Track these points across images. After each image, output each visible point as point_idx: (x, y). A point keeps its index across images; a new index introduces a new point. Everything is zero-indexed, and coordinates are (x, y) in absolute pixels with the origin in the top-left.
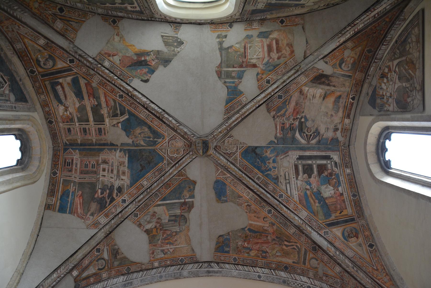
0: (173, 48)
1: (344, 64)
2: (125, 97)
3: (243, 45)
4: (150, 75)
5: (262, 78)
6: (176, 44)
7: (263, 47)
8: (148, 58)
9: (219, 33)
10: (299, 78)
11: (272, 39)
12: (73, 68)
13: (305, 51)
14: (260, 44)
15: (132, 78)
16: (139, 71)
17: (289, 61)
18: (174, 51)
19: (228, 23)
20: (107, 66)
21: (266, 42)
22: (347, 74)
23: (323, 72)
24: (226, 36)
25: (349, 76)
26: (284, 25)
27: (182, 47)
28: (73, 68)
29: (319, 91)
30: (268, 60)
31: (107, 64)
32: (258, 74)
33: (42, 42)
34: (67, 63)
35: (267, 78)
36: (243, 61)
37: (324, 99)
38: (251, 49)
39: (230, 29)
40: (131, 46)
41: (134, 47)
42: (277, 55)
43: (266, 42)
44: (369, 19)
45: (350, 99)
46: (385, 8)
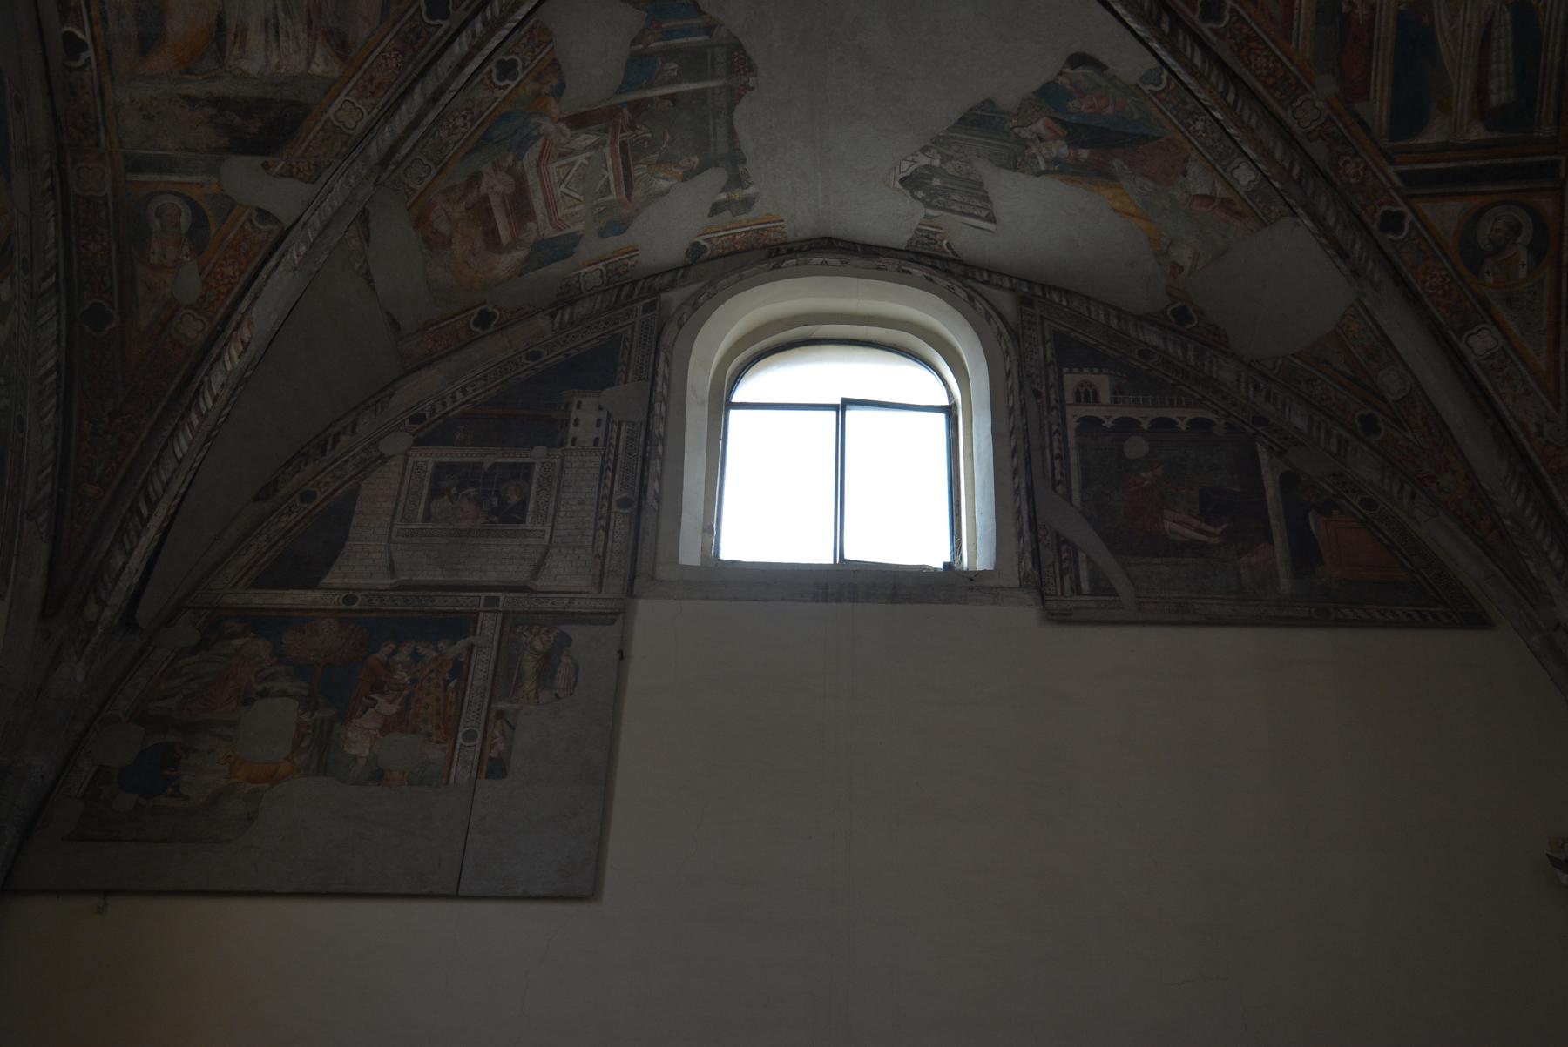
0: (949, 168)
1: (185, 222)
2: (1194, 10)
3: (637, 193)
4: (1062, 80)
5: (538, 79)
6: (936, 182)
7: (550, 204)
8: (1061, 149)
9: (744, 218)
10: (367, 118)
11: (515, 242)
12: (1397, 190)
13: (368, 240)
14: (563, 211)
15: (1146, 88)
16: (1110, 110)
17: (428, 179)
18: (946, 159)
19: (710, 259)
20: (1243, 166)
21: (541, 226)
22: (155, 177)
23: (266, 166)
24: (716, 209)
25: (138, 166)
26: (476, 312)
27: (906, 168)
28: (1397, 190)
29: (261, 61)
30: (519, 158)
31: (1245, 176)
32: (559, 91)
33: (1481, 343)
34: (1416, 214)
35: (513, 84)
36: (633, 128)
37: (221, 23)
38: (601, 183)
39: (700, 240)
40: (1128, 214)
41: (1117, 205)
42: (483, 190)
43: (541, 226)
44: (166, 487)
45: (88, 39)
46: (129, 554)
